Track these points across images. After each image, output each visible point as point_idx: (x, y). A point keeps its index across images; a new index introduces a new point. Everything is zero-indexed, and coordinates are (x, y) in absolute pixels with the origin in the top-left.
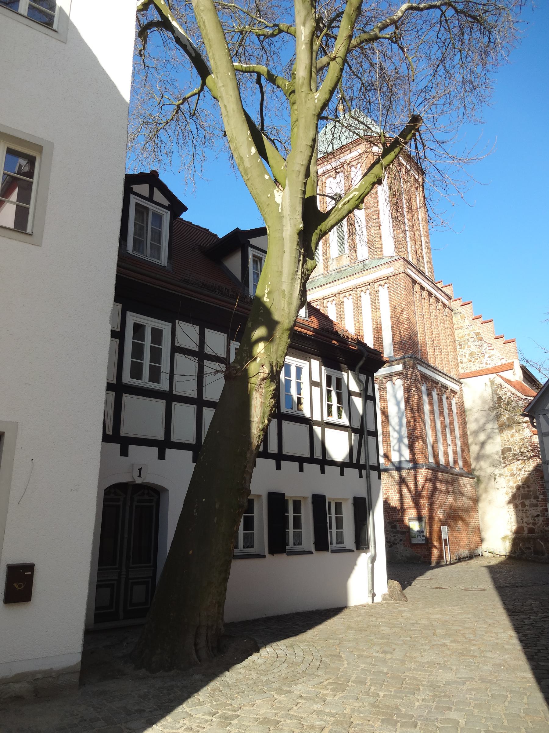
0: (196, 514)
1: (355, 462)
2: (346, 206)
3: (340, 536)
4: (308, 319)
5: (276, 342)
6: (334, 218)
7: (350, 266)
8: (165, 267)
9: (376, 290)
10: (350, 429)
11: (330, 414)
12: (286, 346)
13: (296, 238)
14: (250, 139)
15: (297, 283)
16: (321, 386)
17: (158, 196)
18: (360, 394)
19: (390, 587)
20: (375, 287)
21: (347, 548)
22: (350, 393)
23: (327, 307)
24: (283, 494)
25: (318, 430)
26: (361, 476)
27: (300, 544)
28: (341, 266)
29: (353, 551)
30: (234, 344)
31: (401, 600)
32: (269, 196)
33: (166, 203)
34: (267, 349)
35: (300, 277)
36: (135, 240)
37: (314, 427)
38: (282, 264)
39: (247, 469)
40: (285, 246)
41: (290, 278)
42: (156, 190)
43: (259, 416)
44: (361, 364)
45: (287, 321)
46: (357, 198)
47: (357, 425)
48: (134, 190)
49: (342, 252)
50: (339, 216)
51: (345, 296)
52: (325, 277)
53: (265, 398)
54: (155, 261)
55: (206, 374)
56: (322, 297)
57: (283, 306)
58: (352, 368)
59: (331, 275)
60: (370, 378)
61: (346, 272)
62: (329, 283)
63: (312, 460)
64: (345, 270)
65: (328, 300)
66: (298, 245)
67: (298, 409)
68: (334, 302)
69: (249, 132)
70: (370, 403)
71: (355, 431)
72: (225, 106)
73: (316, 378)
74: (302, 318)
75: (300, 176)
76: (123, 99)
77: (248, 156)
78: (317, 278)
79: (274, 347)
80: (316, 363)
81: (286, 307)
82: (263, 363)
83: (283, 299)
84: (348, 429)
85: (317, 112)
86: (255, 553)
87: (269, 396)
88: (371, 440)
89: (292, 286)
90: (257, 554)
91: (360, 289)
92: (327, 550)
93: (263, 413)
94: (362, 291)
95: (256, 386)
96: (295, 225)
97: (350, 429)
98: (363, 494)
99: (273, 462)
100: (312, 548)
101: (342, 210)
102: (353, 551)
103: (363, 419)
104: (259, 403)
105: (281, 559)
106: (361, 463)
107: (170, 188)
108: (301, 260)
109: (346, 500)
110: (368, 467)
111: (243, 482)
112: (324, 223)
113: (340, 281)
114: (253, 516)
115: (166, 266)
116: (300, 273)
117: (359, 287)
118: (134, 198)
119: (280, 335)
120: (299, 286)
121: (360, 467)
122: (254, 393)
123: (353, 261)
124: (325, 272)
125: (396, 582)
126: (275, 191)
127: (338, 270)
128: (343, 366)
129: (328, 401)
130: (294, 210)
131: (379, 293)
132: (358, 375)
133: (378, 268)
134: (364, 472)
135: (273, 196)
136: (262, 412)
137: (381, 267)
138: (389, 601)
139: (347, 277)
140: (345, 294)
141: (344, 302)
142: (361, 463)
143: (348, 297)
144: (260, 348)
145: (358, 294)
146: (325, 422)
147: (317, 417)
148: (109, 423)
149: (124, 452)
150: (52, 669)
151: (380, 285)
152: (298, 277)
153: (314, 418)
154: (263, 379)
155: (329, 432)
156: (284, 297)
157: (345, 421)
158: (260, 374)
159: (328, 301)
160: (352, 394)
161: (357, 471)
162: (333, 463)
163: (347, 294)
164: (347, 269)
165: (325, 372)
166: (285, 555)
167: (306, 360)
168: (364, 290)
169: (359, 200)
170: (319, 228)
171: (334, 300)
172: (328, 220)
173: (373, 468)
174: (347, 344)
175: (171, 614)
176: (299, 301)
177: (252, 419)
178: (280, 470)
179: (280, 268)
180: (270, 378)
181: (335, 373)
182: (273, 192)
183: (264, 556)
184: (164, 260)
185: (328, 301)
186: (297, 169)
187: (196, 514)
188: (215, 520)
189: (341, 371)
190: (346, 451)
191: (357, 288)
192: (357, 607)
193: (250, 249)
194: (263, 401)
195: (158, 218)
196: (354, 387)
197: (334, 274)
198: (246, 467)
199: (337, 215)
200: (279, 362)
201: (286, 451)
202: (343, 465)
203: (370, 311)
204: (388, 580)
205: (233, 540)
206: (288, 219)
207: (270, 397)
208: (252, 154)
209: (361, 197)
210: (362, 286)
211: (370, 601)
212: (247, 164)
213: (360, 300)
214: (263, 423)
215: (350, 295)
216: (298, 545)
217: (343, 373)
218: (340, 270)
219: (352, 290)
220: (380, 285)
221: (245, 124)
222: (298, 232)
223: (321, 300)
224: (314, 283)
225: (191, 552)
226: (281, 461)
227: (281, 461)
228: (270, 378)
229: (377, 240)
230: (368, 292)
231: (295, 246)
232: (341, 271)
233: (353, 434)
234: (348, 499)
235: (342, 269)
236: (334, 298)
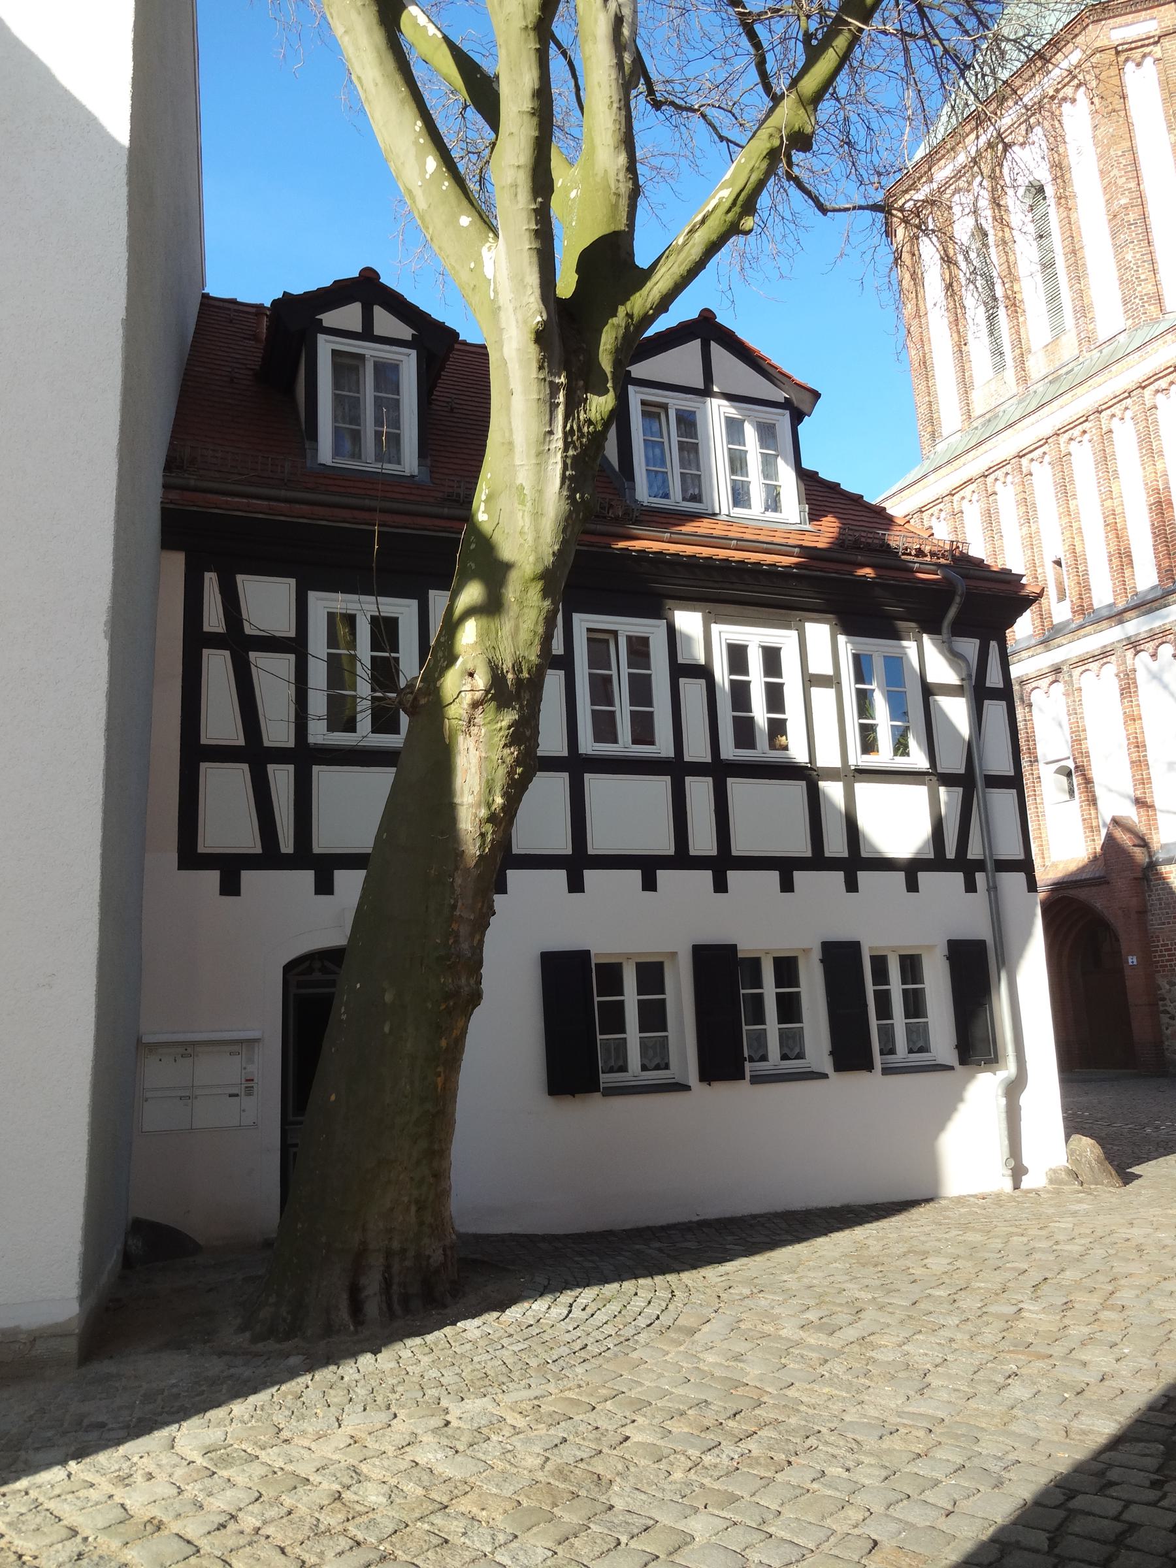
0: (344, 1017)
1: (951, 853)
2: (697, 235)
3: (887, 1035)
4: (808, 527)
5: (511, 614)
6: (667, 276)
7: (1081, 359)
8: (413, 476)
9: (1148, 406)
10: (931, 777)
11: (869, 745)
12: (541, 618)
13: (533, 351)
14: (422, 141)
15: (552, 460)
16: (839, 683)
17: (385, 322)
18: (962, 686)
19: (1071, 1153)
20: (1146, 399)
21: (940, 1061)
22: (928, 691)
23: (1031, 475)
24: (733, 948)
25: (833, 790)
26: (971, 887)
27: (924, 1049)
28: (1057, 364)
29: (952, 1068)
30: (582, 620)
31: (1103, 1184)
32: (472, 265)
33: (405, 332)
34: (483, 635)
35: (560, 444)
36: (337, 433)
37: (822, 784)
38: (510, 423)
39: (457, 913)
40: (511, 379)
41: (533, 452)
42: (378, 311)
43: (477, 789)
44: (952, 613)
45: (532, 559)
46: (728, 204)
47: (953, 763)
48: (325, 324)
49: (1058, 330)
50: (679, 267)
51: (1071, 439)
52: (1020, 402)
53: (490, 747)
54: (390, 468)
55: (361, 711)
56: (1014, 452)
57: (521, 523)
58: (931, 626)
59: (1035, 392)
60: (994, 645)
61: (1070, 376)
62: (1029, 415)
63: (818, 861)
64: (1067, 373)
65: (1030, 456)
66: (541, 368)
67: (773, 746)
68: (1047, 458)
69: (419, 123)
70: (995, 710)
71: (948, 780)
72: (359, 78)
73: (821, 664)
74: (793, 527)
75: (519, 197)
76: (114, 141)
77: (420, 183)
78: (1002, 408)
79: (507, 625)
80: (819, 633)
81: (527, 524)
82: (470, 666)
83: (520, 507)
84: (927, 778)
85: (531, 19)
86: (673, 1081)
87: (499, 740)
88: (1002, 800)
89: (539, 472)
90: (677, 1084)
91: (1108, 412)
92: (738, 1075)
93: (488, 781)
94: (1113, 416)
95: (461, 722)
96: (525, 322)
97: (934, 778)
98: (977, 927)
99: (707, 876)
100: (827, 1065)
101: (687, 248)
102: (952, 1068)
103: (971, 752)
104: (474, 761)
105: (726, 1094)
106: (970, 856)
107: (411, 298)
108: (558, 404)
109: (930, 948)
110: (989, 865)
111: (451, 941)
112: (638, 294)
113: (1055, 404)
114: (798, 993)
115: (416, 472)
116: (559, 434)
117: (1104, 407)
118: (327, 341)
119: (518, 594)
120: (559, 466)
121: (968, 868)
122: (461, 738)
123: (1085, 344)
124: (1021, 388)
125: (1086, 1142)
126: (484, 250)
127: (1050, 378)
128: (902, 625)
129: (861, 715)
130: (518, 281)
131: (1158, 412)
132: (950, 643)
133: (1149, 348)
134: (980, 877)
135: (479, 261)
136: (484, 780)
137: (1155, 345)
138: (1065, 1184)
139: (1071, 389)
140: (1071, 432)
141: (1070, 454)
142: (970, 856)
143: (1079, 439)
144: (469, 634)
145: (1103, 426)
146: (853, 768)
147: (827, 757)
148: (286, 831)
149: (324, 886)
150: (18, 1327)
151: (1157, 391)
152: (552, 446)
153: (820, 763)
154: (475, 705)
155: (863, 790)
156: (522, 503)
157: (917, 759)
158: (463, 694)
159: (1032, 460)
160: (936, 691)
161: (958, 878)
162: (885, 864)
163: (1076, 432)
164: (1072, 370)
165: (849, 646)
166: (598, 1095)
167: (788, 627)
168: (1119, 414)
169: (737, 209)
170: (622, 311)
171: (1045, 453)
172: (649, 285)
173: (1005, 866)
174: (912, 571)
175: (300, 1226)
176: (564, 503)
177: (458, 800)
178: (726, 891)
179: (507, 435)
180: (492, 699)
181: (877, 647)
182: (480, 254)
183: (686, 1088)
184: (410, 462)
185: (1032, 460)
186: (509, 180)
187: (344, 1017)
188: (387, 1029)
189: (900, 638)
190: (925, 830)
191: (1100, 412)
192: (960, 1201)
193: (322, 338)
194: (483, 755)
195: (387, 374)
196: (940, 670)
197: (1041, 389)
198: (454, 907)
199: (676, 265)
200: (524, 657)
201: (740, 846)
202: (912, 869)
203: (1138, 461)
204: (1068, 1137)
205: (440, 1069)
206: (511, 310)
207: (503, 743)
208: (428, 176)
209: (741, 198)
210: (1110, 403)
211: (1007, 1185)
212: (422, 204)
213: (1111, 441)
214: (489, 806)
215: (1085, 432)
216: (657, 1068)
217: (905, 643)
218: (1055, 375)
219: (1086, 420)
220: (1157, 391)
221: (407, 108)
222: (533, 336)
223: (1013, 461)
224: (994, 423)
225: (333, 1098)
226: (729, 873)
227: (795, 873)
228: (492, 699)
229: (1143, 277)
230: (1128, 414)
231: (534, 373)
232: (1059, 377)
233: (942, 790)
234: (934, 947)
235: (1060, 372)
236: (1045, 448)
